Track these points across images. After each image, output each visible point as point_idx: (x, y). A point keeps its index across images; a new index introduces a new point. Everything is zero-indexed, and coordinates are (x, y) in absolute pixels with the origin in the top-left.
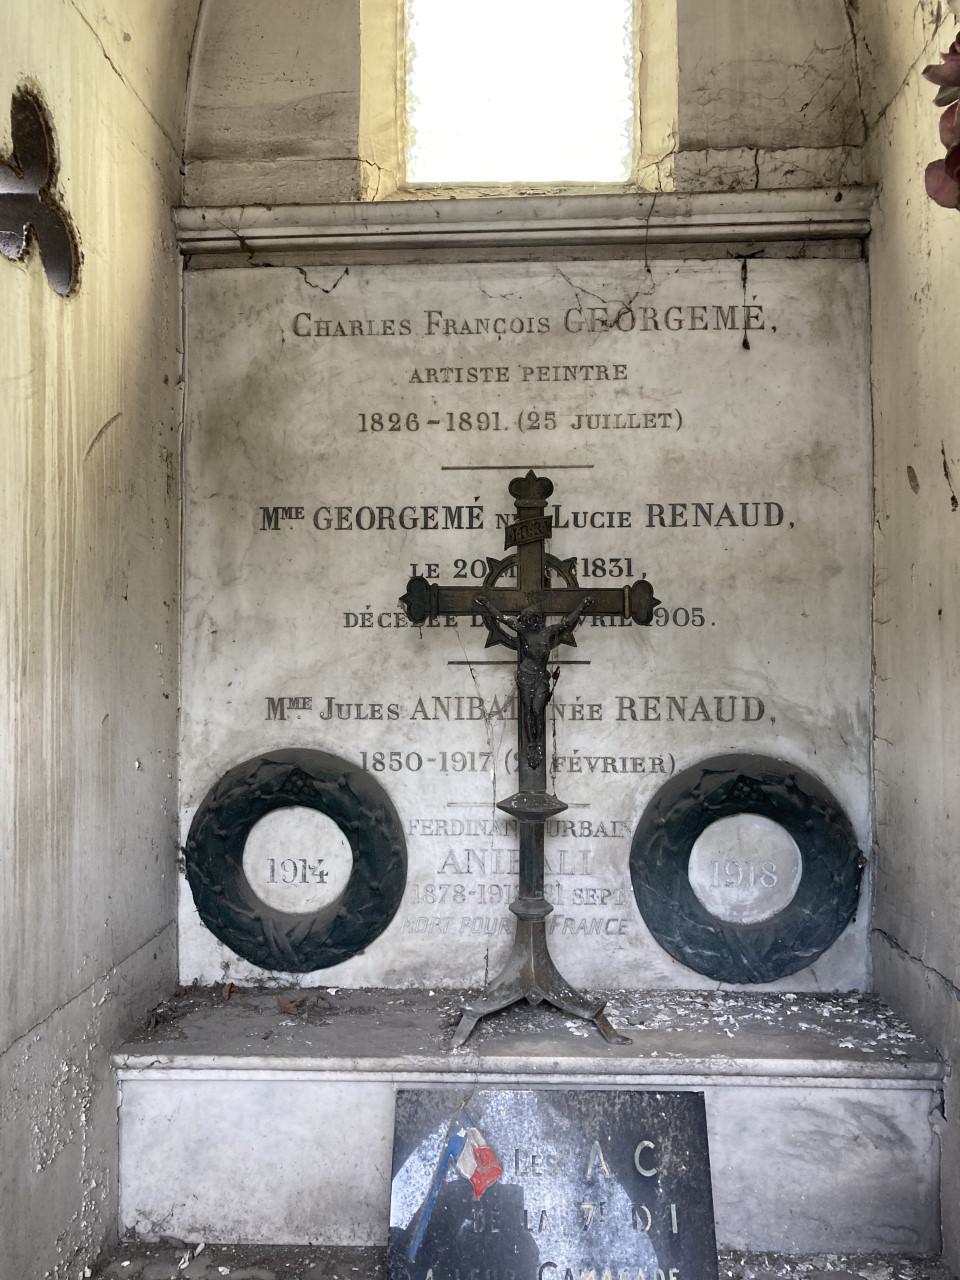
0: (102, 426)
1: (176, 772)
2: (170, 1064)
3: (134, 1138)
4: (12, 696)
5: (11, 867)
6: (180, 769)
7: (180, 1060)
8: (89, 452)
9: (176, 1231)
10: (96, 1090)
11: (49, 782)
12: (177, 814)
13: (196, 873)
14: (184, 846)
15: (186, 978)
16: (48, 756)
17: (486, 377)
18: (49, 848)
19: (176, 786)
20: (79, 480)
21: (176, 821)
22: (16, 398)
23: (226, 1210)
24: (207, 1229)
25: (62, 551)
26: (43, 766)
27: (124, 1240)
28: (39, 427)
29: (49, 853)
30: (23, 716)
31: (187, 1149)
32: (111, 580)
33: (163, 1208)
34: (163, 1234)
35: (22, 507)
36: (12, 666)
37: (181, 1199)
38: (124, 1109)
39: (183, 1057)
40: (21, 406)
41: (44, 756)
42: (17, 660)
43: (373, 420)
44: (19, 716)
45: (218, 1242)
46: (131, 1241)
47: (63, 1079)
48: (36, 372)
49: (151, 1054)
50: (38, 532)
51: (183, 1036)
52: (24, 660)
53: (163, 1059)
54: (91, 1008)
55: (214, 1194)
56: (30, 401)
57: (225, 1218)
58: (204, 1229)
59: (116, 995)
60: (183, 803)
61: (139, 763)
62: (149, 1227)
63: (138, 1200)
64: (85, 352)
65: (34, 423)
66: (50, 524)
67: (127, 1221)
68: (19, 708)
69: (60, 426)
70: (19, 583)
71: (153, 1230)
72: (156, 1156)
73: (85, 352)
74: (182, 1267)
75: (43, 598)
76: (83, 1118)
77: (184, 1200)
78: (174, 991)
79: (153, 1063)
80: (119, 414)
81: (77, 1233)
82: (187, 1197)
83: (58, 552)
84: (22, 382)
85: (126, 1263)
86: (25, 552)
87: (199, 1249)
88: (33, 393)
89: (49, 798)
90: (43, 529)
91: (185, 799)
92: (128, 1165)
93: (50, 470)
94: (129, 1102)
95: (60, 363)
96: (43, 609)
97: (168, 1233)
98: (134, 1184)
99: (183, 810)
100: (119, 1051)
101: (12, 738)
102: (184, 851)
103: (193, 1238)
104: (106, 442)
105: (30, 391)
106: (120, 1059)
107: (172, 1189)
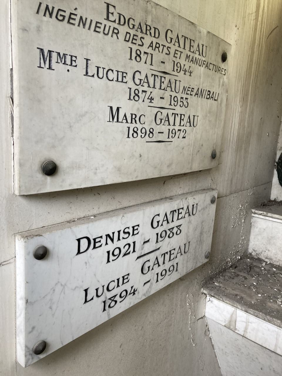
0: (272, 30)
1: (278, 140)
2: (266, 215)
3: (254, 232)
4: (240, 106)
5: (234, 151)
6: (279, 139)
7: (269, 214)
8: (268, 38)
9: (262, 257)
10: (248, 216)
11: (246, 132)
12: (276, 152)
13: (280, 169)
14: (277, 161)
15: (272, 198)
16: (246, 124)
17: (185, 73)
18: (243, 149)
19: (277, 144)
20: (264, 46)
21: (276, 154)
22: (251, 20)
23: (277, 256)
24: (270, 259)
25: (257, 67)
26: (245, 127)
27: (248, 255)
28: (256, 29)
29: (243, 150)
30: (242, 112)
31: (268, 238)
32: (268, 78)
33: (260, 251)
34: (259, 257)
35: (248, 53)
36: (241, 98)
37: (264, 250)
38: (252, 224)
39: (270, 214)
40: (252, 22)
41: (245, 124)
42: (242, 96)
43: (134, 131)
44: (241, 112)
45: (273, 263)
46: (250, 256)
47: (240, 209)
48: (257, 12)
49: (262, 211)
50: (251, 60)
51: (270, 209)
52: (244, 97)
53: (265, 213)
54: (248, 194)
55: (274, 251)
56: (254, 21)
57: (276, 258)
58: (270, 259)
59: (254, 194)
60: (278, 149)
61: (268, 134)
62: (255, 254)
63: (253, 247)
64: (270, 6)
65: (254, 28)
66: (255, 59)
67: (250, 251)
68: (241, 109)
69: (261, 29)
70: (245, 75)
71: (256, 255)
72: (259, 237)
73: (270, 6)
74: (263, 265)
75: (250, 80)
76: (243, 221)
77: (265, 250)
78: (268, 200)
79: (262, 213)
80: (278, 26)
81: (238, 247)
82: (267, 250)
83: (255, 68)
84: (253, 14)
85: (249, 260)
86: (248, 66)
87: (268, 263)
88: (255, 18)
89: (245, 136)
90: (253, 60)
91: (279, 148)
92: (252, 237)
93: (257, 42)
94: (254, 222)
95: (263, 9)
96: (250, 83)
97: (260, 257)
98: (253, 243)
99: (278, 151)
100: (253, 208)
101: (239, 117)
102: (277, 163)
103: (266, 260)
104: (273, 35)
105: (254, 18)
106: (253, 211)
107: (263, 247)
